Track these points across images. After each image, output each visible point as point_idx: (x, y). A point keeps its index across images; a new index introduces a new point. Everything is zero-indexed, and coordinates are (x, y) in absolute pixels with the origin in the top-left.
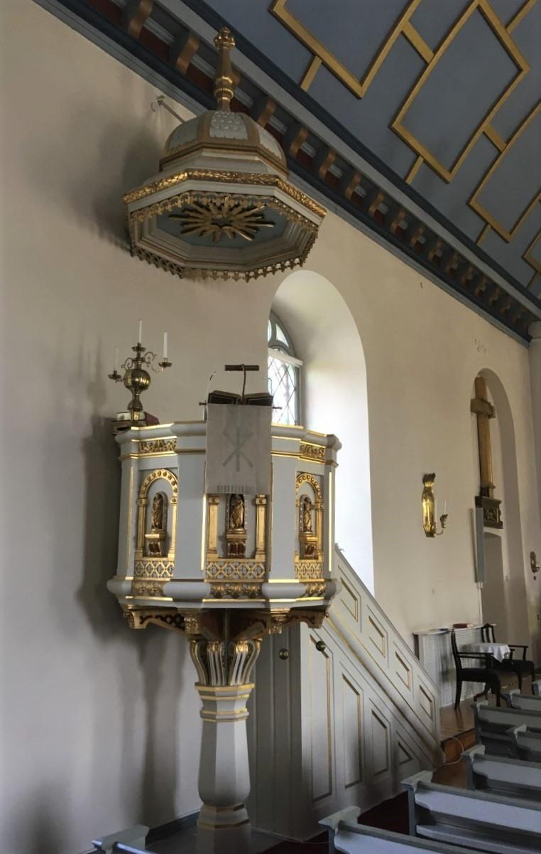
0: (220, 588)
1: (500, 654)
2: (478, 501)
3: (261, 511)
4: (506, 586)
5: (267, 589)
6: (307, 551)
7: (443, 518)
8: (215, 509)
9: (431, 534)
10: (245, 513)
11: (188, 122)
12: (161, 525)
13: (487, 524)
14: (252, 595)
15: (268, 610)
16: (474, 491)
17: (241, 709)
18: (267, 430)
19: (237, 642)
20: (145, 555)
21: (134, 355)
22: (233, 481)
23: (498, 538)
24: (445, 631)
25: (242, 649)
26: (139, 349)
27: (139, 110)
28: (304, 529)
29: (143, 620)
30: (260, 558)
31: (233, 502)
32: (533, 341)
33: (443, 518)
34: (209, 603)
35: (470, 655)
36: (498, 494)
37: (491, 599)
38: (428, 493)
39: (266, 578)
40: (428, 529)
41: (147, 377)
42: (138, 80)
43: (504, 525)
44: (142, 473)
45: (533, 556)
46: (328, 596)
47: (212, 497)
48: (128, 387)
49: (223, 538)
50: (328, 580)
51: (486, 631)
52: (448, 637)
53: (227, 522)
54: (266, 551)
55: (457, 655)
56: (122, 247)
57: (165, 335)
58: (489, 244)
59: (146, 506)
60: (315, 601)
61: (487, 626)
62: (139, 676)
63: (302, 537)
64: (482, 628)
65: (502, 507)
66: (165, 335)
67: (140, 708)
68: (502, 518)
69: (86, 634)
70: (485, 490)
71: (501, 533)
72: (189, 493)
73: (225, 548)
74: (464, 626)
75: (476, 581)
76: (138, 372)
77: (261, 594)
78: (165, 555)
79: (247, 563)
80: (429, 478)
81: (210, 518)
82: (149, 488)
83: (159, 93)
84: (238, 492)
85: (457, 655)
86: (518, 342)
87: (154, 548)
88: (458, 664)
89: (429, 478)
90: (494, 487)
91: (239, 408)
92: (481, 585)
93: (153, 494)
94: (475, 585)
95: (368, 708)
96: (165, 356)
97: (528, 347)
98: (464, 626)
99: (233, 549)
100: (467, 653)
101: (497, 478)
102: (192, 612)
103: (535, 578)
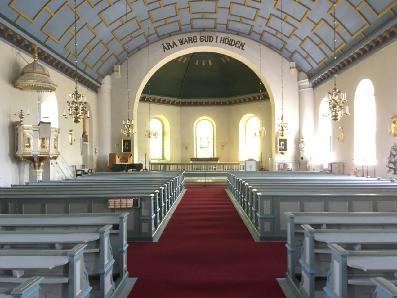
0: (41, 153)
1: (86, 171)
2: (83, 136)
3: (48, 141)
4: (88, 156)
5: (49, 153)
6: (55, 147)
7: (74, 140)
8: (40, 140)
9: (71, 144)
10: (45, 141)
11: (159, 241)
12: (29, 142)
13: (85, 141)
14: (47, 154)
15: (49, 156)
16: (82, 133)
17: (41, 174)
18: (50, 128)
19: (41, 163)
20: (25, 148)
21: (21, 111)
22: (43, 136)
23: (87, 145)
24: (73, 166)
25: (42, 164)
26: (22, 110)
27: (15, 56)
28: (55, 144)
29: (24, 159)
30: (48, 148)
31: (43, 139)
32: (98, 93)
33: (74, 140)
34: (39, 156)
35: (143, 46)
36: (87, 134)
37: (85, 159)
38: (71, 134)
39: (49, 152)
40: (71, 143)
41: (23, 115)
42: (14, 49)
43: (89, 142)
44: (24, 134)
45: (96, 149)
46: (58, 155)
47: (40, 139)
48: (20, 118)
49: (42, 145)
50: (58, 152)
51: (83, 166)
52: (75, 167)
53: (42, 142)
54: (49, 147)
55: (76, 171)
56: (12, 86)
57: (28, 109)
58: (88, 70)
59: (25, 139)
60: (56, 156)
61: (83, 165)
62: (18, 170)
63: (55, 146)
64: (82, 166)
65: (88, 137)
66: (28, 109)
67: (18, 176)
68: (88, 140)
69: (10, 162)
70: (84, 133)
71: (88, 143)
72: (35, 137)
73: (42, 147)
74: (78, 165)
75: (81, 155)
76: (22, 115)
77: (48, 154)
78: (30, 148)
79: (45, 149)
80: (71, 131)
81: (39, 142)
82: (26, 136)
83: (18, 51)
84: (44, 138)
85: (76, 171)
86: (95, 93)
87: (27, 147)
88: (77, 173)
89: (71, 131)
90: (86, 132)
91: (45, 124)
92: (82, 156)
93: (27, 137)
94: (81, 156)
95: (61, 177)
96: (28, 112)
97: (97, 94)
98: (78, 165)
99: (43, 147)
100: (79, 171)
101: (87, 130)
102: (36, 157)
103: (96, 155)
